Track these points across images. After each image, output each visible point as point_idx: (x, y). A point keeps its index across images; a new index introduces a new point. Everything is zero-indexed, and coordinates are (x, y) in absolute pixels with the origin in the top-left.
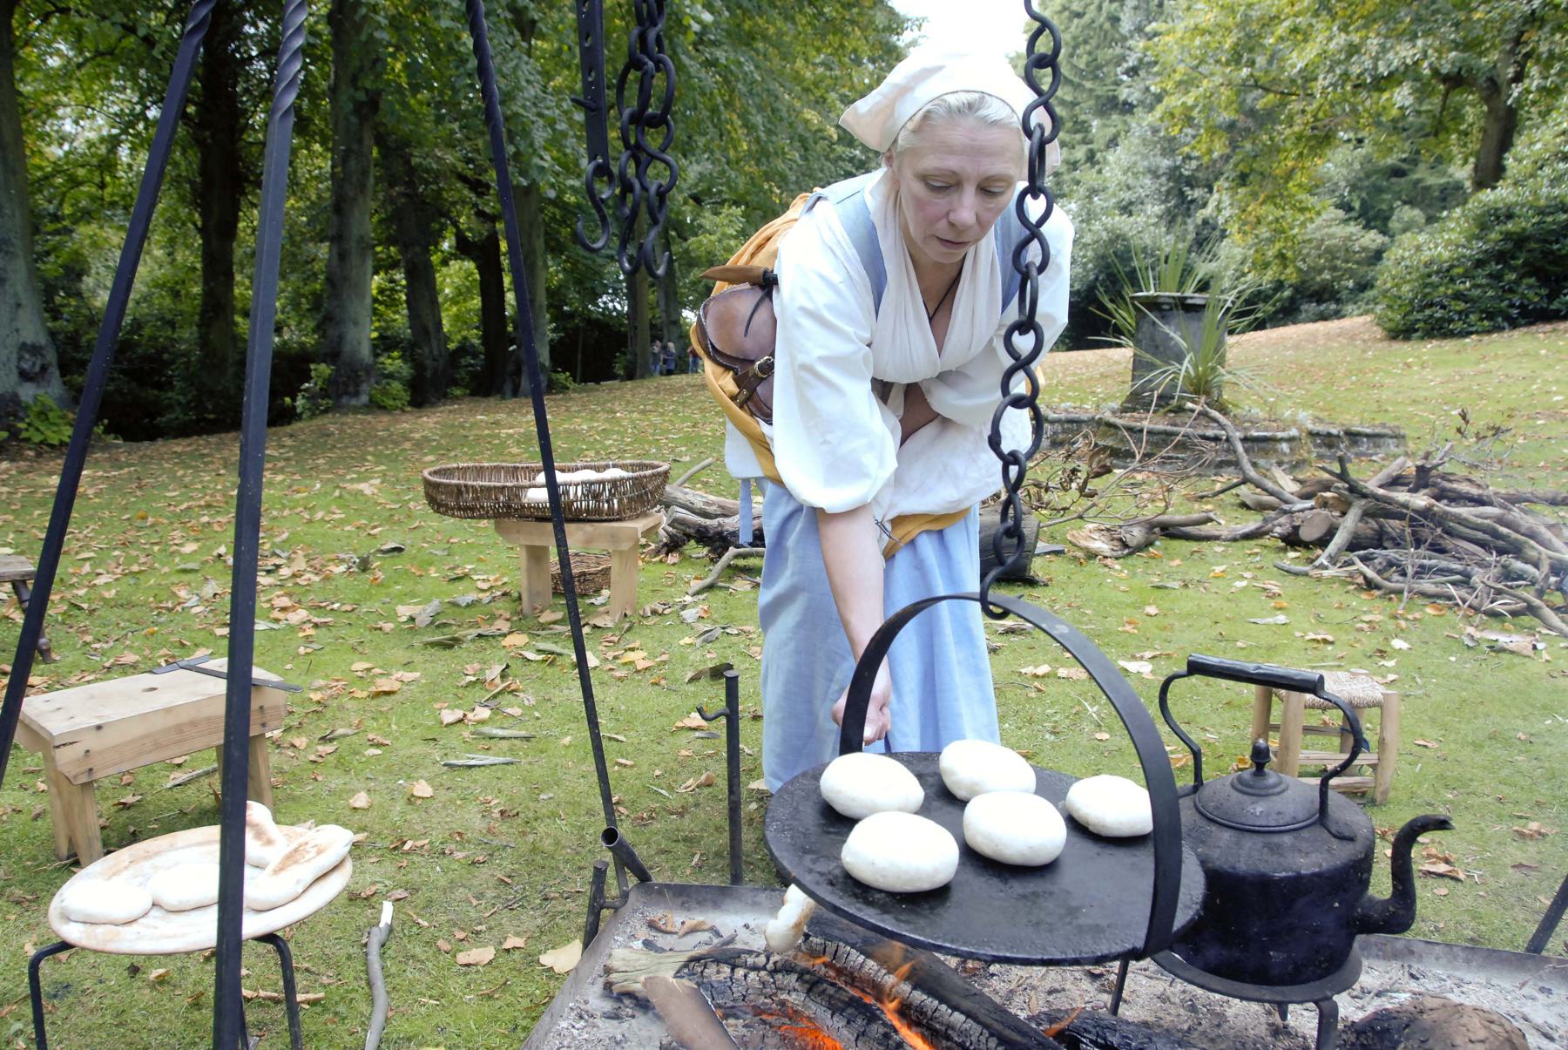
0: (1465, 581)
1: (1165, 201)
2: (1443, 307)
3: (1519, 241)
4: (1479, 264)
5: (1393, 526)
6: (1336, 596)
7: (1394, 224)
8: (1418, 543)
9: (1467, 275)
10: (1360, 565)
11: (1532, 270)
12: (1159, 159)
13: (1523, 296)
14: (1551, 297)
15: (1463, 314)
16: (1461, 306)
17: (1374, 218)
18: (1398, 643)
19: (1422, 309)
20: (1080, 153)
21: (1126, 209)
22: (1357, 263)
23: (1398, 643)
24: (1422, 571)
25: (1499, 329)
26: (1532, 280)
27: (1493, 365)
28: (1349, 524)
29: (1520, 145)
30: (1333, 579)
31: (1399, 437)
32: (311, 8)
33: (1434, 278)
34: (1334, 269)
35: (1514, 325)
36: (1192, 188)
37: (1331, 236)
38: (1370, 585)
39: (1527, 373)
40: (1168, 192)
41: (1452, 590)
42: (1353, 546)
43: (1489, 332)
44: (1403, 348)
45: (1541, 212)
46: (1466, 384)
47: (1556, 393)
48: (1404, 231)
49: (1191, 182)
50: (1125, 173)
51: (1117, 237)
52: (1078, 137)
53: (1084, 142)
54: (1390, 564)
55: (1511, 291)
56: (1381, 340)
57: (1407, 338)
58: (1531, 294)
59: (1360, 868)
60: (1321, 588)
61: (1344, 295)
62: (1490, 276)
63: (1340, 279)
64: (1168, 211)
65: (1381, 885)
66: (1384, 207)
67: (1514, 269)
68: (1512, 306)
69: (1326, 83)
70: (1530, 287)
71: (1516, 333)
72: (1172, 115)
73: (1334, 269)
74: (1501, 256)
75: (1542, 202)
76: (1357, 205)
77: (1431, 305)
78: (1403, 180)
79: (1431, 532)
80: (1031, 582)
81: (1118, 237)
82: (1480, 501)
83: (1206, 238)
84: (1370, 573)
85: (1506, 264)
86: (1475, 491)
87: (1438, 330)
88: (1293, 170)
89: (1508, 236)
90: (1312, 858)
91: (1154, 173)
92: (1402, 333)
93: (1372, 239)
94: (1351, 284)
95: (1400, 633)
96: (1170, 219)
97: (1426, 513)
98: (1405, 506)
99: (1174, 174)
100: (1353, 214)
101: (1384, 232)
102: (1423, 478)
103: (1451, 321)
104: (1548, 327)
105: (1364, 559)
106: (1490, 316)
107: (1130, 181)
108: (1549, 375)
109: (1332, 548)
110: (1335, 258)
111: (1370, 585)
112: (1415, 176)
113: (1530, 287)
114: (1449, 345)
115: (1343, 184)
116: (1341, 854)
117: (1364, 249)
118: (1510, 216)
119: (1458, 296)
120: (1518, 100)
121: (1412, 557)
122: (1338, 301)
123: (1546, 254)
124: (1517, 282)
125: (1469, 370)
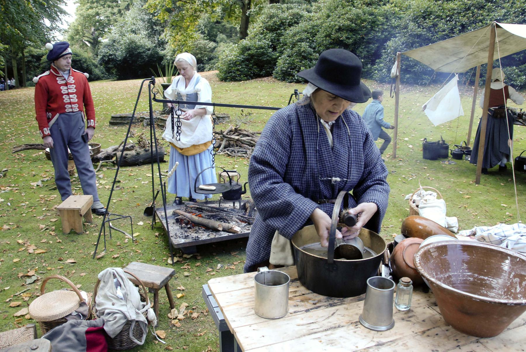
0: (246, 153)
1: (147, 30)
2: (234, 73)
3: (252, 56)
4: (243, 62)
5: (232, 142)
6: (223, 158)
7: (218, 39)
8: (237, 146)
9: (240, 65)
10: (227, 152)
11: (256, 64)
12: (144, 16)
13: (254, 71)
14: (261, 71)
15: (240, 75)
16: (239, 73)
17: (212, 37)
18: (236, 166)
19: (229, 73)
20: (116, 10)
21: (134, 32)
22: (208, 52)
23: (236, 166)
24: (238, 151)
25: (249, 79)
26: (256, 67)
27: (247, 91)
28: (224, 143)
29: (251, 27)
30: (222, 155)
31: (229, 117)
32: (524, 301)
33: (232, 65)
34: (201, 53)
35: (252, 78)
36: (156, 26)
37: (200, 44)
38: (229, 155)
39: (255, 93)
40: (148, 27)
41: (244, 155)
42: (225, 148)
43: (246, 80)
44: (225, 84)
45: (257, 49)
46: (241, 97)
47: (263, 100)
48: (221, 42)
49: (155, 24)
50: (133, 19)
51: (133, 42)
52: (115, 4)
53: (117, 6)
54: (233, 151)
55: (251, 69)
56: (218, 81)
57: (225, 81)
58: (255, 70)
59: (241, 188)
60: (220, 157)
61: (205, 62)
62: (245, 65)
63: (203, 57)
64: (149, 33)
65: (243, 190)
66: (214, 33)
67: (251, 63)
68: (251, 73)
69: (199, 4)
70: (255, 68)
71: (253, 81)
72: (151, 6)
73: (201, 53)
74: (247, 60)
75: (257, 46)
76: (206, 32)
77: (231, 72)
78: (219, 25)
79: (238, 143)
80: (165, 162)
81: (132, 42)
82: (248, 136)
83: (162, 44)
84: (229, 153)
85: (249, 62)
86: (246, 133)
87: (234, 79)
88: (189, 26)
89: (249, 55)
90: (237, 188)
91: (143, 20)
92: (224, 79)
93: (212, 44)
94: (207, 58)
95: (236, 164)
96: (149, 36)
97: (238, 140)
98: (234, 139)
99: (149, 21)
100: (206, 35)
101: (215, 41)
102: (236, 131)
103: (236, 77)
104: (260, 79)
105: (228, 150)
106: (246, 76)
107: (135, 22)
108: (261, 94)
109: (221, 148)
110: (201, 50)
111: (229, 155)
112: (223, 24)
113: (255, 68)
114: (236, 84)
115: (202, 25)
116: (240, 187)
117: (210, 48)
118: (249, 49)
119: (238, 70)
120: (249, 14)
121: (236, 149)
122: (203, 64)
123: (258, 60)
124: (252, 67)
125: (242, 92)
